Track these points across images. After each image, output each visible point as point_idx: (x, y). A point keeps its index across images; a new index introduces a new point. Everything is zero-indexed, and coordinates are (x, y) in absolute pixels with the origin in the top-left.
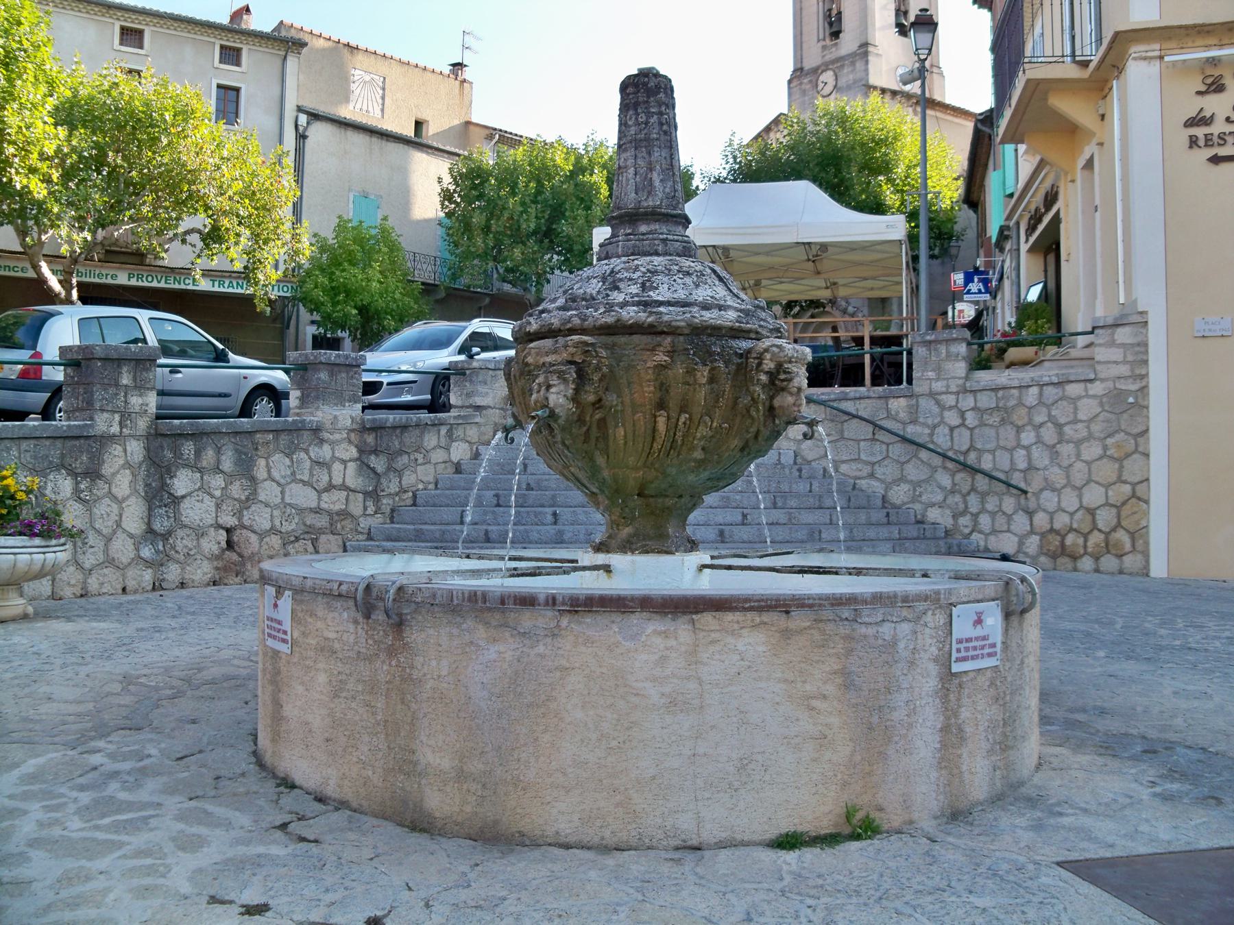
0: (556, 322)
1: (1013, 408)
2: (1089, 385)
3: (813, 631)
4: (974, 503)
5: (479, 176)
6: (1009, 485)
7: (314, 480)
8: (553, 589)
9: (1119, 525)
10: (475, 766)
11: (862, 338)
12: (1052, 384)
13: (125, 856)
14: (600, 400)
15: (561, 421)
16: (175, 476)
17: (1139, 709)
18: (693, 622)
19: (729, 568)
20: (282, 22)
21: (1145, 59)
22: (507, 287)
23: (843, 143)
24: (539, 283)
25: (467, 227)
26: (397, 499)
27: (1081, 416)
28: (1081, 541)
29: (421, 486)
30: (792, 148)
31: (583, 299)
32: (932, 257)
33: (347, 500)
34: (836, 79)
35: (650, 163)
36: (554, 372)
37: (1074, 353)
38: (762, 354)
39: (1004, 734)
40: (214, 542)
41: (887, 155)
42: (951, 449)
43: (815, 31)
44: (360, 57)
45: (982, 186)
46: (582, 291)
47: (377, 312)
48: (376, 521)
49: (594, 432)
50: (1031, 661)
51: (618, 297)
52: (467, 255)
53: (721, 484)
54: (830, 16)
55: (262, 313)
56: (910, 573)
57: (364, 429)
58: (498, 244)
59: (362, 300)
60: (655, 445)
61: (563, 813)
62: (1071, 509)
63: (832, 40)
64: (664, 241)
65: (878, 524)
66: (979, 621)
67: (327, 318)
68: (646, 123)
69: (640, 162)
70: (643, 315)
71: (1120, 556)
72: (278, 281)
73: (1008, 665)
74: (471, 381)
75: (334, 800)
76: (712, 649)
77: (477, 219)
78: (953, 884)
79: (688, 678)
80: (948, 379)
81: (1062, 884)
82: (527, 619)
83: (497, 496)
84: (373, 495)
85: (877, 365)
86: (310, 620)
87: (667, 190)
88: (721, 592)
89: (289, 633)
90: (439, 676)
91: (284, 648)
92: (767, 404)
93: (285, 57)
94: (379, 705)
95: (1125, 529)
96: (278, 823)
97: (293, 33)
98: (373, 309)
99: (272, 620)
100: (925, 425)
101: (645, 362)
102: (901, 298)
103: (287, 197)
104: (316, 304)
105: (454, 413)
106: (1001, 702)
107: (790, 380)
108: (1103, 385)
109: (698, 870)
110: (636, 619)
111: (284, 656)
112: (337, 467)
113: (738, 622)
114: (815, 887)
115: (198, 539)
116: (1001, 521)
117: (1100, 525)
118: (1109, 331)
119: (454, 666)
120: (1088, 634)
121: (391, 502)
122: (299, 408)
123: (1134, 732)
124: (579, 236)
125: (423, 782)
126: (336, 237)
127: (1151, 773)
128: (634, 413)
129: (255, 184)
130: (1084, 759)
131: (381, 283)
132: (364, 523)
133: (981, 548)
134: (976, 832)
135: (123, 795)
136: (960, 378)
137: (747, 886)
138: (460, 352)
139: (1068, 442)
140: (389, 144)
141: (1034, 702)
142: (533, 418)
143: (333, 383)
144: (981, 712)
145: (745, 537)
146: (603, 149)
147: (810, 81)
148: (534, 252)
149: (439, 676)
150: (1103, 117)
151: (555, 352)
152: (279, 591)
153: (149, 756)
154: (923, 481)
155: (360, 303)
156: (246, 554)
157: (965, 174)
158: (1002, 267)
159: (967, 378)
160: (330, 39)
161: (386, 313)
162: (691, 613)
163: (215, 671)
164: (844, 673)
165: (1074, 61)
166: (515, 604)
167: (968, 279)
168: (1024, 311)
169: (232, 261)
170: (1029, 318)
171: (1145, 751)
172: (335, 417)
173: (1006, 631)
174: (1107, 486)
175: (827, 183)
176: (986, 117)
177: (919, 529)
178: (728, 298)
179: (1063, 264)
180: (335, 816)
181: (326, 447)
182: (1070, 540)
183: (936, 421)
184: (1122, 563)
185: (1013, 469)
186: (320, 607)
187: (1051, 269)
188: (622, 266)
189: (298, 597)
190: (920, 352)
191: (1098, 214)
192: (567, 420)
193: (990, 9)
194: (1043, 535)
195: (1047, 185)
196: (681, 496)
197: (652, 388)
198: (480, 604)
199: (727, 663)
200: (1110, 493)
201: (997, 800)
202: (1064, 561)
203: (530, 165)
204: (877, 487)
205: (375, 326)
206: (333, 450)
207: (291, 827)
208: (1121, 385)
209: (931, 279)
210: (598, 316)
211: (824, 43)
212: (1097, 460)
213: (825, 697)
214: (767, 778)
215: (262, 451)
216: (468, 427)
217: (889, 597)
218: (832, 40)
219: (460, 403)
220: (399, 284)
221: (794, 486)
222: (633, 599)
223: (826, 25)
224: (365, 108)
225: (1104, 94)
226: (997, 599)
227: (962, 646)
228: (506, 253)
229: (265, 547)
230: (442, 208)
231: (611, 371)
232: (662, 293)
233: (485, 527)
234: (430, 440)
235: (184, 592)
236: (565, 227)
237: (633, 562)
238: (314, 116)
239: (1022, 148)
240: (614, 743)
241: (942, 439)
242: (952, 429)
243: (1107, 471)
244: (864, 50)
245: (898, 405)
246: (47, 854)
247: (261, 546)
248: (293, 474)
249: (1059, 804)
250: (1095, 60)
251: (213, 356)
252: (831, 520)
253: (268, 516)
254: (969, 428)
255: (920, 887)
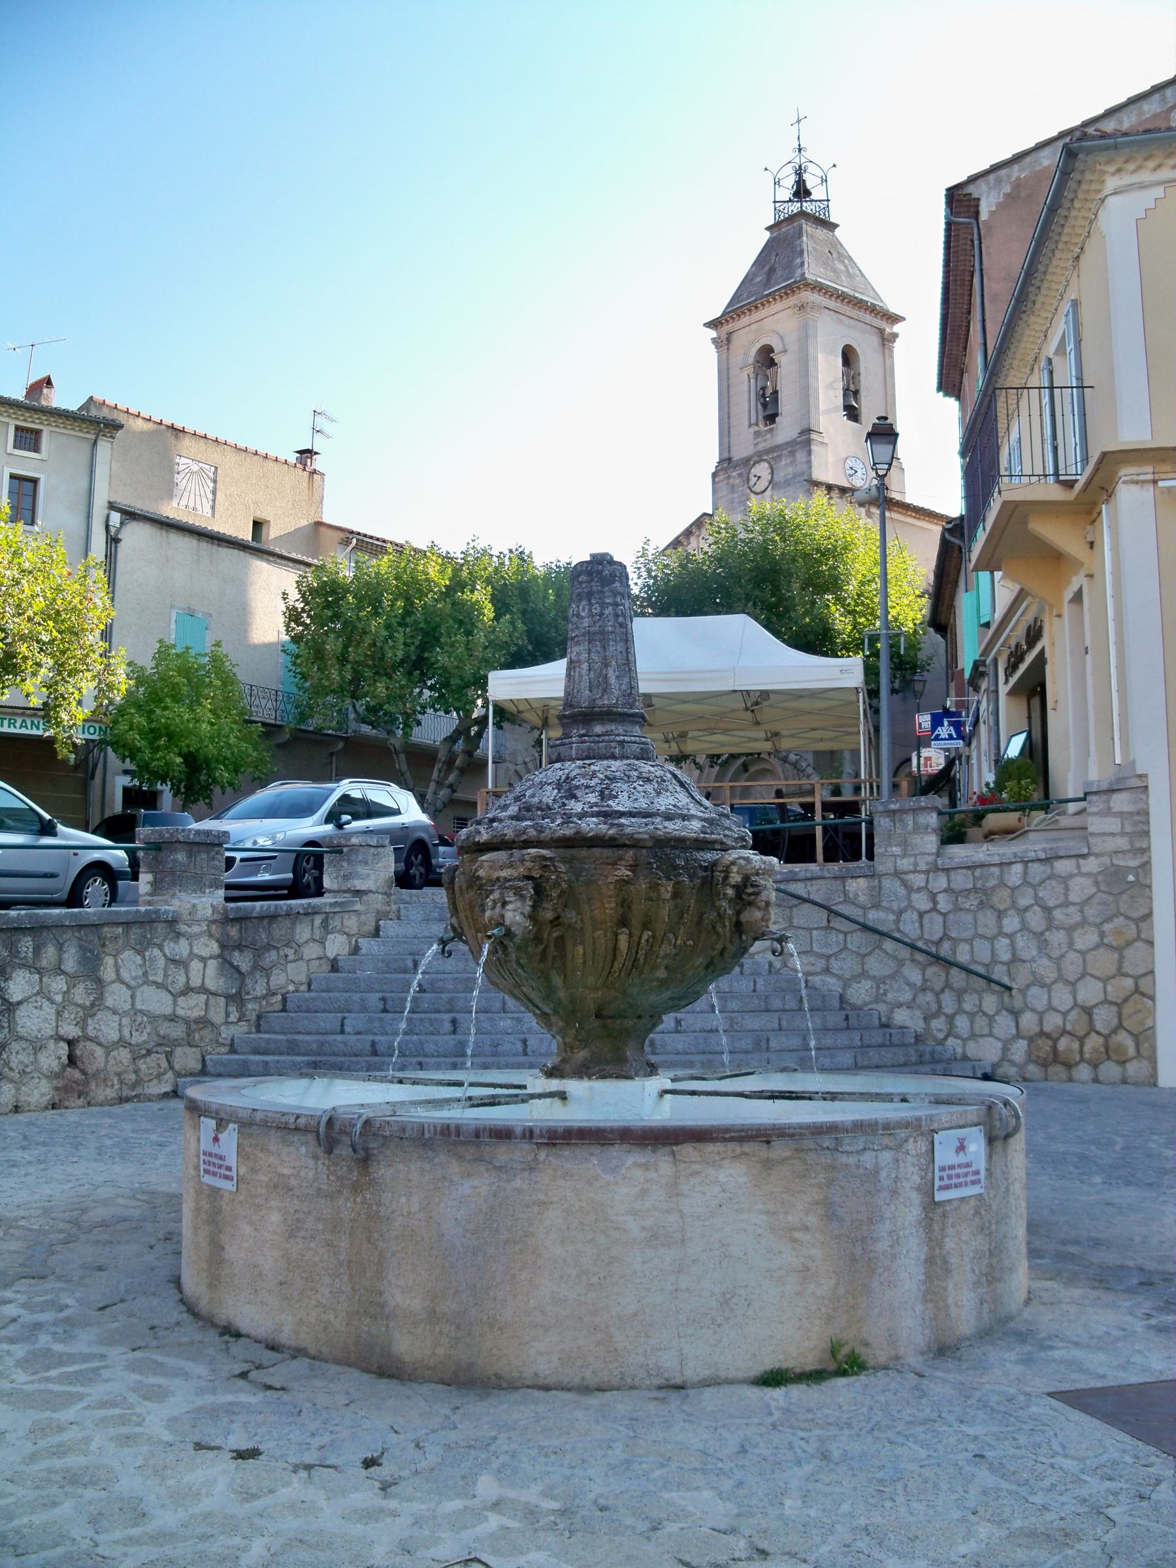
0: (509, 834)
1: (994, 888)
2: (1081, 861)
3: (794, 1161)
4: (948, 1002)
5: (333, 592)
6: (990, 980)
7: (169, 981)
8: (531, 1121)
9: (1120, 1026)
10: (448, 1306)
11: (813, 805)
12: (1039, 860)
13: (89, 1407)
14: (558, 918)
15: (517, 940)
16: (10, 978)
17: (1137, 1239)
18: (673, 1154)
19: (693, 1093)
20: (91, 398)
21: (1137, 482)
22: (366, 729)
23: (783, 554)
24: (407, 725)
25: (319, 655)
26: (264, 1003)
27: (1073, 898)
28: (1076, 1045)
29: (291, 988)
30: (720, 560)
31: (539, 809)
32: (893, 691)
33: (206, 1004)
34: (772, 473)
35: (605, 658)
36: (511, 888)
37: (1064, 821)
38: (728, 867)
39: (991, 1266)
40: (53, 1057)
41: (835, 569)
42: (921, 938)
43: (747, 413)
44: (187, 442)
45: (951, 607)
46: (536, 799)
47: (207, 761)
48: (239, 1031)
49: (552, 951)
50: (1017, 1188)
51: (577, 807)
52: (319, 691)
53: (683, 1003)
54: (764, 396)
55: (65, 762)
56: (888, 1098)
57: (227, 920)
58: (356, 679)
59: (188, 746)
60: (616, 964)
61: (542, 1354)
62: (1064, 1008)
63: (766, 425)
64: (622, 743)
65: (836, 1029)
66: (961, 1148)
67: (144, 767)
68: (601, 614)
69: (594, 656)
70: (603, 827)
71: (1122, 1063)
72: (84, 720)
73: (992, 1193)
74: (349, 861)
75: (289, 1348)
76: (692, 1181)
77: (332, 646)
78: (944, 1415)
79: (669, 1211)
80: (915, 856)
81: (1051, 1412)
82: (503, 1153)
83: (384, 999)
84: (237, 999)
85: (831, 837)
86: (260, 1155)
87: (623, 687)
88: (700, 1123)
89: (234, 1169)
90: (409, 1213)
91: (229, 1186)
92: (734, 919)
93: (95, 442)
94: (343, 1244)
95: (1127, 1031)
96: (237, 1372)
97: (105, 413)
98: (201, 757)
99: (210, 1155)
100: (889, 910)
101: (606, 876)
102: (855, 753)
103: (99, 618)
104: (130, 750)
105: (327, 899)
106: (987, 1232)
107: (758, 894)
108: (1098, 861)
109: (686, 1408)
110: (615, 1151)
111: (226, 1194)
112: (196, 965)
113: (719, 1153)
114: (806, 1421)
115: (35, 1054)
116: (981, 1024)
117: (1099, 1026)
118: (1104, 797)
119: (426, 1202)
120: (1083, 1158)
121: (257, 1007)
122: (152, 894)
123: (1131, 1263)
124: (457, 667)
125: (391, 1325)
126: (157, 667)
127: (1147, 1305)
128: (595, 929)
129: (59, 602)
130: (1076, 1293)
131: (212, 724)
132: (226, 1033)
133: (959, 1056)
134: (964, 1367)
135: (58, 1347)
136: (929, 854)
137: (737, 1421)
138: (327, 821)
139: (1058, 929)
140: (221, 549)
141: (1020, 1231)
142: (489, 937)
143: (192, 865)
144: (966, 1242)
145: (680, 1047)
146: (486, 560)
147: (740, 475)
148: (402, 687)
149: (409, 1213)
150: (1092, 544)
151: (511, 865)
152: (221, 1124)
153: (67, 1306)
154: (889, 977)
155: (185, 750)
156: (90, 1071)
157: (931, 590)
158: (978, 709)
159: (938, 854)
160: (149, 420)
161: (217, 761)
162: (671, 1144)
163: (100, 1213)
164: (827, 1203)
165: (1058, 481)
166: (491, 1137)
167: (937, 722)
168: (1005, 769)
169: (28, 695)
170: (1010, 778)
171: (1142, 1284)
172: (194, 906)
173: (990, 1157)
174: (1105, 981)
175: (763, 602)
176: (955, 526)
177: (884, 1035)
178: (691, 805)
179: (1050, 713)
180: (295, 1365)
181: (183, 942)
182: (1063, 1043)
183: (902, 905)
184: (1125, 1070)
185: (994, 961)
186: (273, 1142)
187: (1036, 715)
188: (578, 771)
189: (246, 1130)
190: (882, 824)
191: (1088, 657)
192: (523, 939)
193: (958, 398)
194: (1031, 1040)
195: (1029, 618)
196: (640, 1017)
197: (613, 905)
198: (453, 1138)
199: (708, 1194)
200: (1109, 988)
201: (985, 1334)
202: (1057, 1070)
203: (396, 579)
204: (833, 985)
205: (202, 778)
206: (191, 945)
207: (253, 1375)
208: (1120, 861)
209: (893, 720)
210: (555, 827)
211: (757, 428)
212: (1094, 949)
213: (807, 1229)
214: (750, 1313)
215: (110, 947)
216: (346, 916)
217: (870, 1125)
218: (766, 425)
219: (335, 887)
220: (234, 726)
221: (735, 984)
222: (612, 1130)
223: (760, 406)
224: (191, 505)
225: (1093, 517)
226: (979, 1124)
227: (944, 1174)
228: (366, 688)
229: (112, 1062)
230: (287, 631)
231: (570, 887)
232: (622, 803)
233: (371, 1037)
234: (303, 932)
235: (20, 1117)
236: (440, 657)
237: (590, 1088)
238: (130, 515)
239: (998, 575)
240: (594, 1279)
241: (909, 927)
242: (921, 915)
243: (1104, 962)
244: (805, 438)
245: (858, 887)
246: (5, 1407)
247: (107, 1061)
248: (145, 974)
249: (1050, 1338)
250: (1082, 480)
251: (37, 827)
252: (780, 1025)
253: (115, 1025)
254: (941, 914)
255: (911, 1419)
